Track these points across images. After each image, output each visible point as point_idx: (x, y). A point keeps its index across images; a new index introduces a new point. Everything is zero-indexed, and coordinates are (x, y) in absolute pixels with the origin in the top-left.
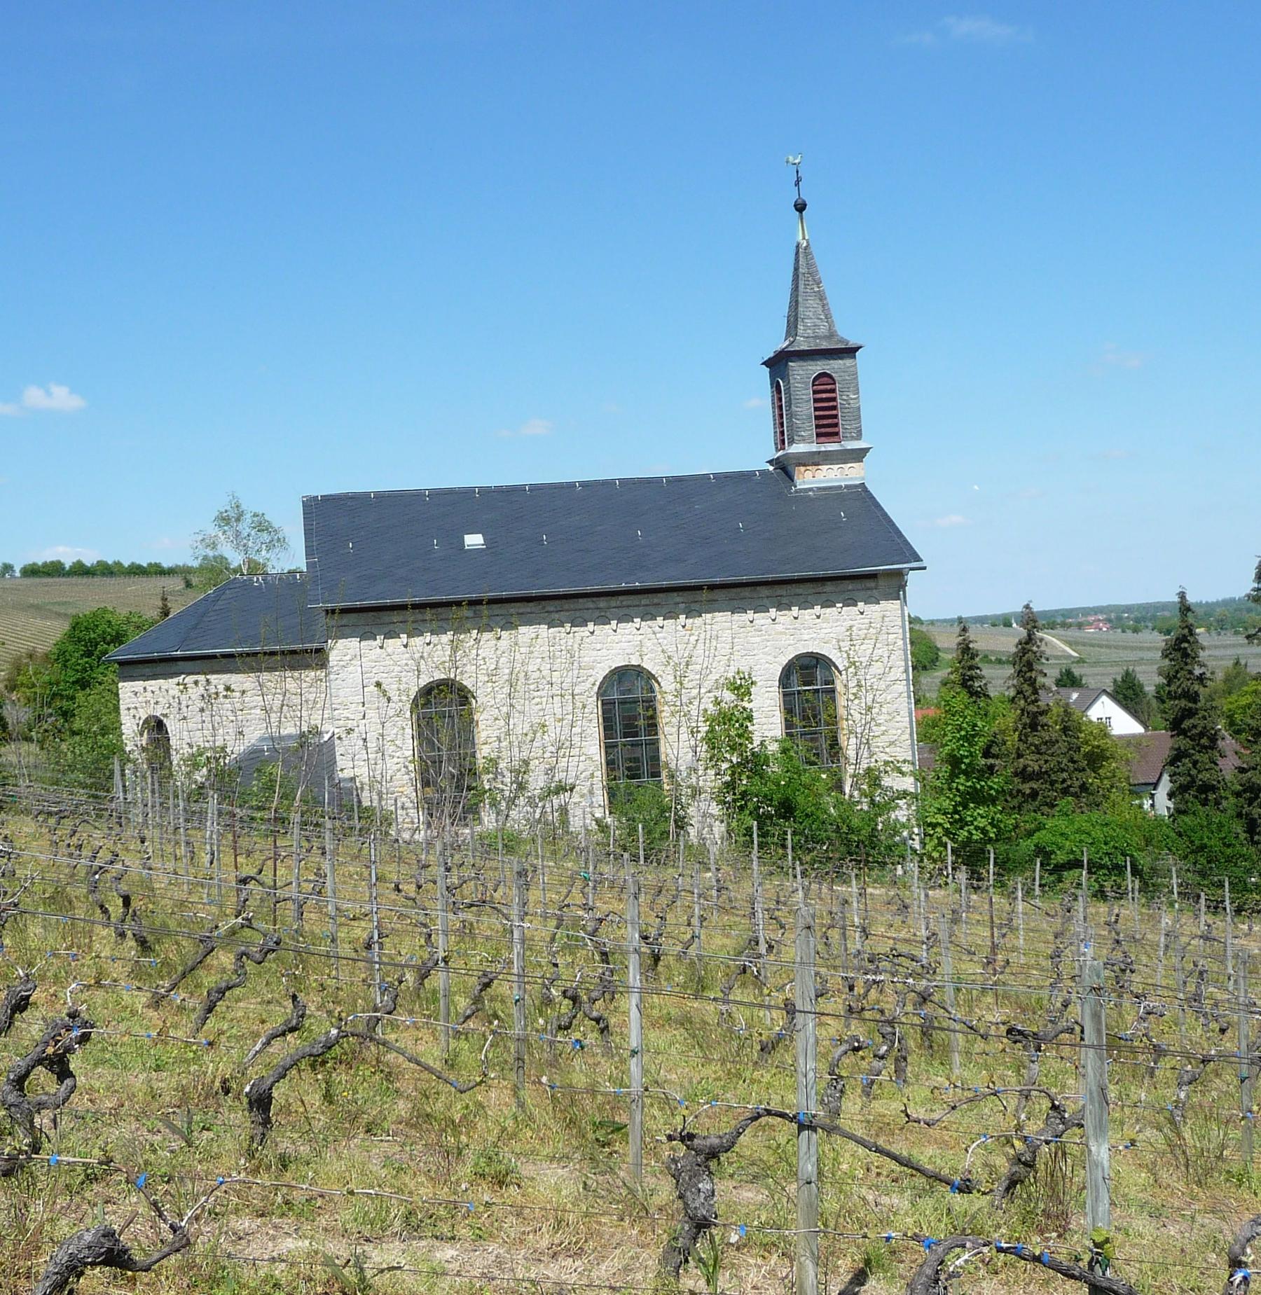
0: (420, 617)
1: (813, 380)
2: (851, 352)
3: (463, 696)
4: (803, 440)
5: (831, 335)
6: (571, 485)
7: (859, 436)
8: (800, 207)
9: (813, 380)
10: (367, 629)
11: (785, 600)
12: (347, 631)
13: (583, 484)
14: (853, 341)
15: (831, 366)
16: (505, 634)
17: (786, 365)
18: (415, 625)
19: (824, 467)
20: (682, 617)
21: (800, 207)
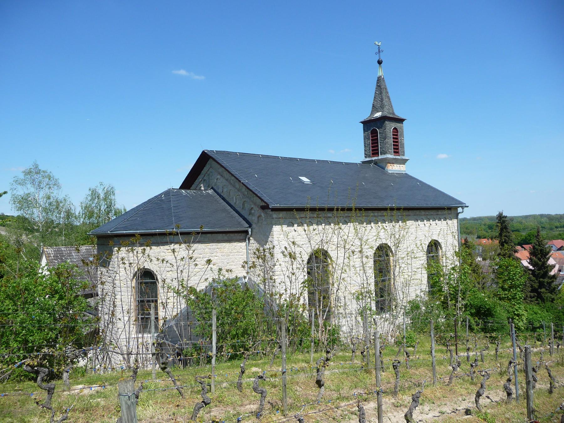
0: (312, 215)
1: (381, 131)
2: (401, 121)
3: (326, 254)
4: (390, 153)
5: (393, 114)
6: (314, 161)
7: (404, 155)
8: (380, 62)
9: (381, 131)
10: (290, 220)
11: (428, 217)
12: (282, 221)
13: (318, 161)
14: (402, 117)
15: (398, 125)
16: (343, 227)
17: (384, 122)
18: (310, 220)
19: (395, 165)
20: (332, 224)
21: (380, 62)
